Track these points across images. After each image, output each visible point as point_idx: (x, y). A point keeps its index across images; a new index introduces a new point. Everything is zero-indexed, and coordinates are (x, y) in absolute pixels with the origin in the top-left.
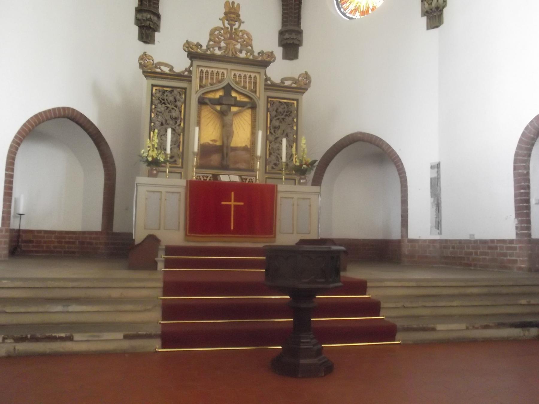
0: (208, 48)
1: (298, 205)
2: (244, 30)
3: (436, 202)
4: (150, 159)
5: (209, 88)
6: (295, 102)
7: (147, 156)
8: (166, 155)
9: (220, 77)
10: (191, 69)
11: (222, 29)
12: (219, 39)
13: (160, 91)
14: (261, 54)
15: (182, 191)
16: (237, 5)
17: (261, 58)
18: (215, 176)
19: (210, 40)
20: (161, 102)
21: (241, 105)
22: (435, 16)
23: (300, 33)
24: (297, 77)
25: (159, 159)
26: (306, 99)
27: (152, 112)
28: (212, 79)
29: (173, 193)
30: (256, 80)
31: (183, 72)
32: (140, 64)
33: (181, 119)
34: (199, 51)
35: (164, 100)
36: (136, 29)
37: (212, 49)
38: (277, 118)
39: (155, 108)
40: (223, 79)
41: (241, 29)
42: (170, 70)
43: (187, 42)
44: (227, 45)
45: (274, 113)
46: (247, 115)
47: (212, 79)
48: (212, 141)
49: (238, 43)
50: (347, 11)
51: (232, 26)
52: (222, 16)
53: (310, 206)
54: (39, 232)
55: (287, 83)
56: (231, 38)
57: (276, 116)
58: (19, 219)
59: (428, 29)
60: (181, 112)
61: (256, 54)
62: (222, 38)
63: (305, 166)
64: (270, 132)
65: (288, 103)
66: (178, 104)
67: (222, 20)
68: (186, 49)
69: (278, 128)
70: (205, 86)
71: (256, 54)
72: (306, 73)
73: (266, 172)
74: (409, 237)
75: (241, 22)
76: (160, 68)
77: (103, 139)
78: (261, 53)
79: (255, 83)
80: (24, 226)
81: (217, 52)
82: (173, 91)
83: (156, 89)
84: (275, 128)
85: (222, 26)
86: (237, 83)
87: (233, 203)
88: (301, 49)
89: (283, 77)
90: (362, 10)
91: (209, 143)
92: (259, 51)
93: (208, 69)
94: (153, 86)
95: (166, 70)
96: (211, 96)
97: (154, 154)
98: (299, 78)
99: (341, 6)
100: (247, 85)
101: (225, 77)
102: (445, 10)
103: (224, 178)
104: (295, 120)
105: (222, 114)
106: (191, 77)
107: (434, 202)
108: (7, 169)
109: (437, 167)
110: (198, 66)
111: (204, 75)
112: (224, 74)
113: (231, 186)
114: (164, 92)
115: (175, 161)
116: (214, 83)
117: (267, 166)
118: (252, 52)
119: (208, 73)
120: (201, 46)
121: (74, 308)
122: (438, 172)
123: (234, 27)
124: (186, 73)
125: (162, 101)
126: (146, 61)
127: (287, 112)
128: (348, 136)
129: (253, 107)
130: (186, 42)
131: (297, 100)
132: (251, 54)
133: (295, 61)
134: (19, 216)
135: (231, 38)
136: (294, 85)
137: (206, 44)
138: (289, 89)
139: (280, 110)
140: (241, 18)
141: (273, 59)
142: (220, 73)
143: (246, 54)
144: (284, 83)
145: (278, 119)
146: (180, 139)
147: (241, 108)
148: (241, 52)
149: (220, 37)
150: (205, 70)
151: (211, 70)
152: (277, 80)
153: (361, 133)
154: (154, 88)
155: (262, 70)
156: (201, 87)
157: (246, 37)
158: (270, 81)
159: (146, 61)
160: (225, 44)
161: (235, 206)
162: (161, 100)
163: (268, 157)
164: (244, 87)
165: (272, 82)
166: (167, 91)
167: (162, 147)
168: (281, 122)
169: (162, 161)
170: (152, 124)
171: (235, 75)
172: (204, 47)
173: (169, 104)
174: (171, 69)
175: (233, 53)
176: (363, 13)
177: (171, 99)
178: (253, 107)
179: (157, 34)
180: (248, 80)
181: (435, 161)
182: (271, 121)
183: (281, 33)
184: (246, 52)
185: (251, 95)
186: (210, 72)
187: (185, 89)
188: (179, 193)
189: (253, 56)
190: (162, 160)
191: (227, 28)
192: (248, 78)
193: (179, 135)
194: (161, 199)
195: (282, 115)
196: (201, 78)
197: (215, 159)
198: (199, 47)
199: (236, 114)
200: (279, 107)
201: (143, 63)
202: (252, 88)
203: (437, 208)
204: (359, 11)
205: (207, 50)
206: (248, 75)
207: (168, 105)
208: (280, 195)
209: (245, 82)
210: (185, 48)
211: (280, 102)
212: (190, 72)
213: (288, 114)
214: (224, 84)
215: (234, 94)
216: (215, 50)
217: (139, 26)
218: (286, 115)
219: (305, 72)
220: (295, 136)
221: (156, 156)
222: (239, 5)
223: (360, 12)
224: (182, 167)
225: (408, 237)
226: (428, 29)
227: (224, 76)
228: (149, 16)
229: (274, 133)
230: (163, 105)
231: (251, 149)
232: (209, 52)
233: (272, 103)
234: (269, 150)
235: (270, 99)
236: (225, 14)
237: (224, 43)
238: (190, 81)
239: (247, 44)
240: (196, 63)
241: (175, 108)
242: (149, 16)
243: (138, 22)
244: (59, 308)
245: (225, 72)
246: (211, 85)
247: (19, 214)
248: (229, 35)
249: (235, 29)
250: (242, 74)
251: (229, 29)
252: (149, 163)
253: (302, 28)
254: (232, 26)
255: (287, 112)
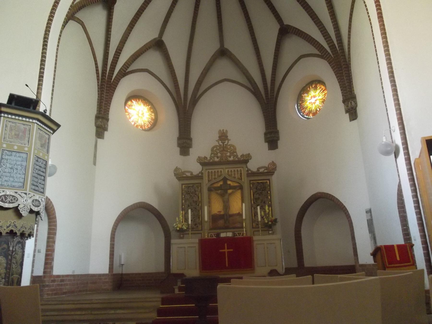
0: (211, 158)
1: (267, 248)
2: (231, 144)
3: (373, 236)
4: (178, 229)
5: (214, 181)
6: (268, 181)
7: (177, 227)
8: (188, 225)
9: (219, 174)
10: (203, 172)
11: (218, 146)
12: (216, 152)
13: (186, 187)
14: (242, 156)
15: (197, 246)
16: (226, 131)
17: (242, 158)
18: (218, 235)
19: (212, 154)
20: (187, 193)
21: (234, 188)
22: (352, 113)
23: (277, 132)
24: (267, 166)
25: (183, 228)
26: (275, 179)
27: (183, 200)
28: (215, 175)
29: (192, 247)
30: (241, 172)
31: (198, 174)
32: (175, 174)
33: (199, 201)
34: (206, 161)
35: (189, 192)
36: (178, 149)
37: (213, 159)
38: (257, 193)
39: (184, 197)
40: (222, 174)
41: (229, 144)
42: (191, 174)
43: (199, 157)
44: (222, 155)
45: (255, 190)
46: (238, 194)
47: (215, 175)
48: (219, 212)
49: (227, 152)
50: (304, 114)
51: (223, 143)
52: (218, 138)
53: (275, 248)
54: (133, 274)
55: (261, 170)
56: (224, 150)
57: (256, 192)
58: (122, 267)
59: (351, 121)
60: (199, 198)
61: (239, 156)
62: (218, 151)
63: (270, 223)
64: (254, 202)
65: (263, 182)
66: (197, 193)
67: (218, 141)
68: (199, 161)
69: (259, 198)
70: (211, 180)
71: (239, 156)
72: (273, 162)
73: (253, 228)
74: (352, 264)
75: (229, 140)
76: (185, 174)
77: (162, 217)
78: (242, 156)
79: (241, 174)
80: (125, 271)
81: (216, 159)
82: (193, 186)
83: (184, 186)
84: (256, 199)
85: (218, 144)
86: (229, 175)
87: (226, 250)
88: (279, 142)
89: (258, 167)
90: (313, 112)
91: (216, 213)
92: (241, 155)
93: (212, 170)
94: (182, 185)
95: (189, 174)
96: (216, 185)
97: (180, 226)
98: (268, 166)
99: (300, 111)
100: (236, 176)
101: (222, 173)
102: (357, 108)
103: (223, 235)
104: (269, 192)
105: (222, 195)
106: (202, 176)
107: (372, 236)
108: (111, 241)
109: (369, 212)
110: (206, 169)
111: (210, 174)
112: (222, 172)
113: (227, 239)
114: (189, 187)
115: (197, 227)
116: (216, 178)
117: (254, 224)
118: (237, 156)
119: (212, 172)
120: (207, 158)
121: (118, 311)
122: (371, 215)
123: (225, 144)
124: (200, 175)
125: (188, 193)
126: (178, 172)
127: (263, 188)
128: (312, 196)
129: (241, 188)
130: (198, 157)
131: (269, 180)
132: (236, 157)
133: (276, 150)
134: (122, 265)
135: (224, 150)
136: (266, 171)
137: (210, 156)
138: (262, 174)
139: (259, 187)
140: (229, 138)
141: (250, 158)
142: (219, 172)
143: (233, 158)
144: (259, 171)
145: (258, 193)
146: (199, 213)
147: (234, 190)
148: (230, 157)
149: (217, 151)
150: (210, 171)
151: (214, 170)
152: (254, 170)
153: (320, 193)
154: (183, 186)
155: (244, 166)
156: (209, 181)
157: (232, 148)
158: (250, 171)
159: (178, 172)
160: (221, 154)
161: (228, 252)
162: (187, 192)
163: (253, 218)
164: (235, 178)
165: (252, 171)
166: (190, 186)
167: (186, 220)
168: (260, 195)
169: (185, 229)
170: (183, 207)
171: (228, 171)
172: (209, 158)
173: (192, 194)
174: (192, 173)
175: (225, 159)
176: (314, 114)
177: (193, 190)
178: (241, 188)
179: (191, 149)
180: (236, 173)
181: (368, 207)
182: (253, 195)
183: (266, 134)
184: (233, 157)
185: (240, 181)
186: (213, 172)
187: (200, 183)
188: (195, 247)
189: (238, 158)
190: (186, 228)
191: (221, 145)
192: (236, 172)
193: (199, 211)
194: (185, 251)
195: (260, 190)
196: (209, 176)
197: (221, 223)
198: (206, 158)
199: (230, 194)
200: (258, 185)
201: (176, 173)
202: (239, 177)
203: (374, 240)
204: (312, 113)
205: (210, 160)
206: (236, 169)
207: (191, 194)
208: (255, 243)
209: (235, 174)
210: (198, 161)
211: (258, 183)
212: (202, 173)
213: (264, 189)
214: (222, 178)
215: (229, 182)
216: (215, 159)
217: (180, 147)
218: (263, 190)
219: (272, 162)
220: (270, 203)
221: (181, 227)
222: (227, 131)
223: (312, 114)
224: (202, 230)
225: (359, 263)
226: (351, 121)
227: (222, 173)
228: (184, 141)
229: (256, 202)
230: (189, 195)
231: (240, 215)
232: (211, 161)
233: (253, 184)
234: (254, 213)
235: (251, 182)
236: (220, 137)
237: (220, 154)
238: (202, 179)
239: (234, 152)
240: (205, 168)
241: (195, 196)
242: (184, 141)
243: (179, 145)
244: (112, 312)
245: (222, 170)
246: (214, 179)
247: (122, 265)
248: (222, 149)
249: (225, 145)
250: (233, 170)
251: (222, 146)
252: (178, 231)
253: (278, 129)
254: (223, 143)
255: (263, 188)
